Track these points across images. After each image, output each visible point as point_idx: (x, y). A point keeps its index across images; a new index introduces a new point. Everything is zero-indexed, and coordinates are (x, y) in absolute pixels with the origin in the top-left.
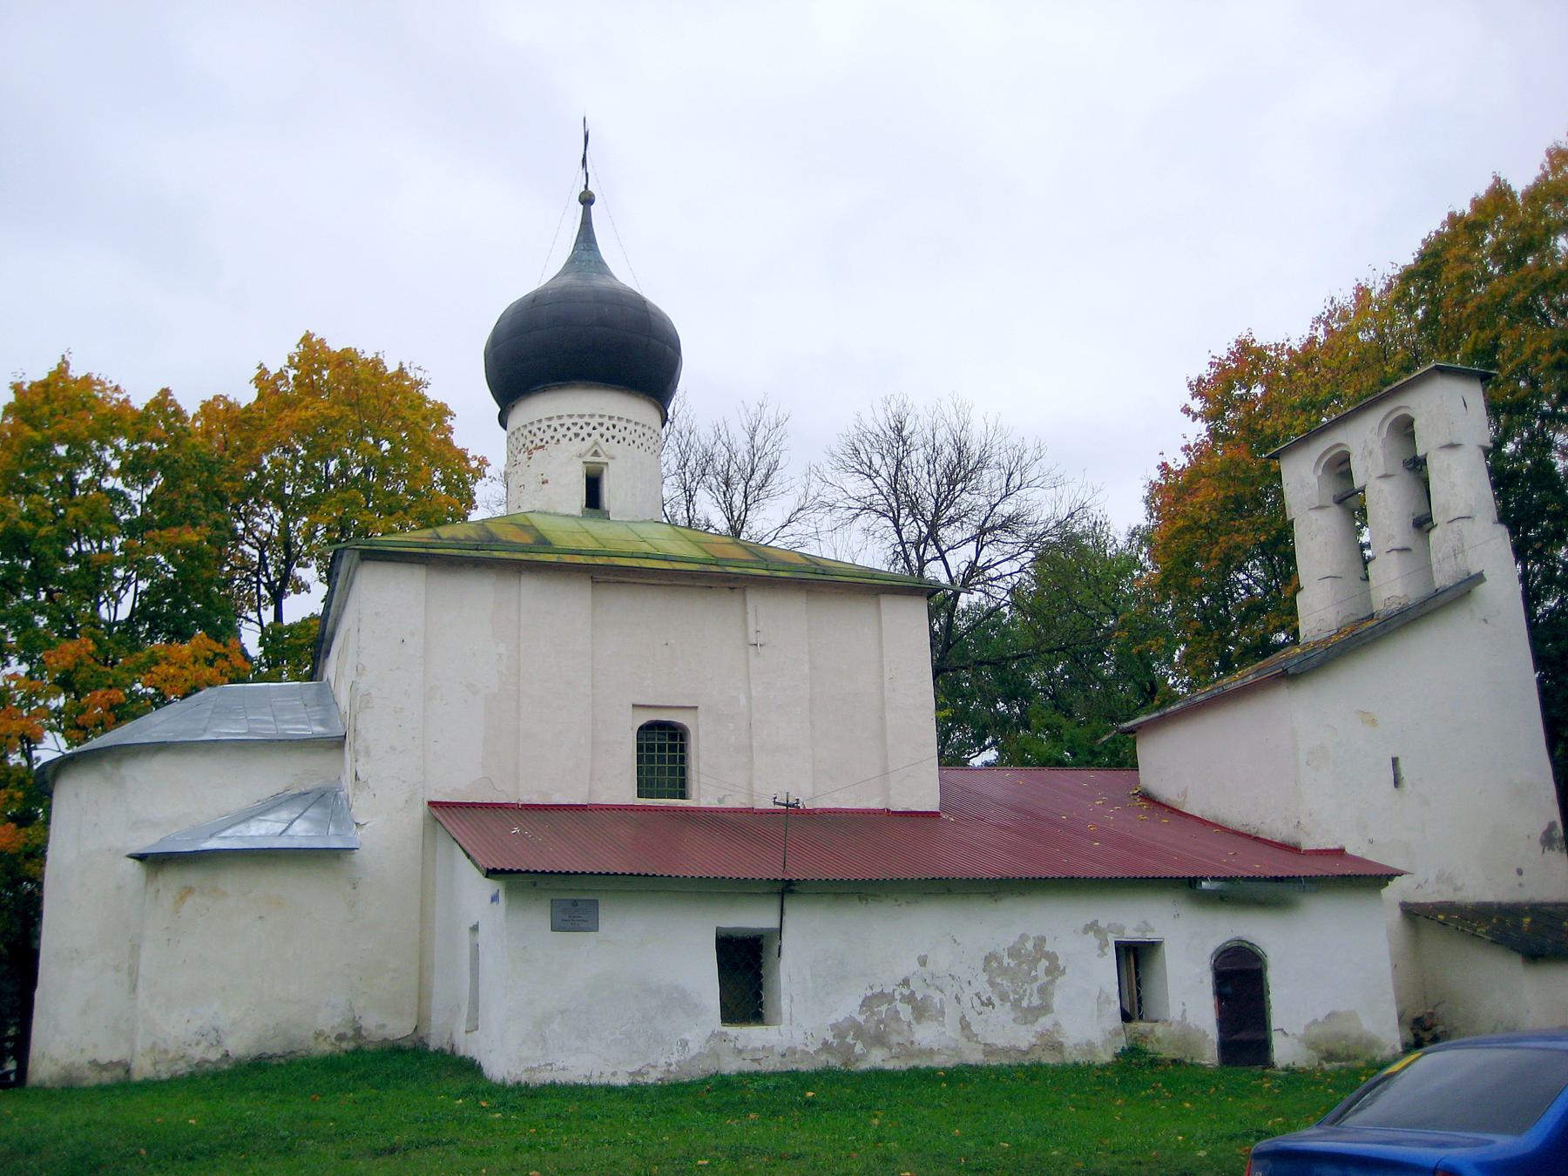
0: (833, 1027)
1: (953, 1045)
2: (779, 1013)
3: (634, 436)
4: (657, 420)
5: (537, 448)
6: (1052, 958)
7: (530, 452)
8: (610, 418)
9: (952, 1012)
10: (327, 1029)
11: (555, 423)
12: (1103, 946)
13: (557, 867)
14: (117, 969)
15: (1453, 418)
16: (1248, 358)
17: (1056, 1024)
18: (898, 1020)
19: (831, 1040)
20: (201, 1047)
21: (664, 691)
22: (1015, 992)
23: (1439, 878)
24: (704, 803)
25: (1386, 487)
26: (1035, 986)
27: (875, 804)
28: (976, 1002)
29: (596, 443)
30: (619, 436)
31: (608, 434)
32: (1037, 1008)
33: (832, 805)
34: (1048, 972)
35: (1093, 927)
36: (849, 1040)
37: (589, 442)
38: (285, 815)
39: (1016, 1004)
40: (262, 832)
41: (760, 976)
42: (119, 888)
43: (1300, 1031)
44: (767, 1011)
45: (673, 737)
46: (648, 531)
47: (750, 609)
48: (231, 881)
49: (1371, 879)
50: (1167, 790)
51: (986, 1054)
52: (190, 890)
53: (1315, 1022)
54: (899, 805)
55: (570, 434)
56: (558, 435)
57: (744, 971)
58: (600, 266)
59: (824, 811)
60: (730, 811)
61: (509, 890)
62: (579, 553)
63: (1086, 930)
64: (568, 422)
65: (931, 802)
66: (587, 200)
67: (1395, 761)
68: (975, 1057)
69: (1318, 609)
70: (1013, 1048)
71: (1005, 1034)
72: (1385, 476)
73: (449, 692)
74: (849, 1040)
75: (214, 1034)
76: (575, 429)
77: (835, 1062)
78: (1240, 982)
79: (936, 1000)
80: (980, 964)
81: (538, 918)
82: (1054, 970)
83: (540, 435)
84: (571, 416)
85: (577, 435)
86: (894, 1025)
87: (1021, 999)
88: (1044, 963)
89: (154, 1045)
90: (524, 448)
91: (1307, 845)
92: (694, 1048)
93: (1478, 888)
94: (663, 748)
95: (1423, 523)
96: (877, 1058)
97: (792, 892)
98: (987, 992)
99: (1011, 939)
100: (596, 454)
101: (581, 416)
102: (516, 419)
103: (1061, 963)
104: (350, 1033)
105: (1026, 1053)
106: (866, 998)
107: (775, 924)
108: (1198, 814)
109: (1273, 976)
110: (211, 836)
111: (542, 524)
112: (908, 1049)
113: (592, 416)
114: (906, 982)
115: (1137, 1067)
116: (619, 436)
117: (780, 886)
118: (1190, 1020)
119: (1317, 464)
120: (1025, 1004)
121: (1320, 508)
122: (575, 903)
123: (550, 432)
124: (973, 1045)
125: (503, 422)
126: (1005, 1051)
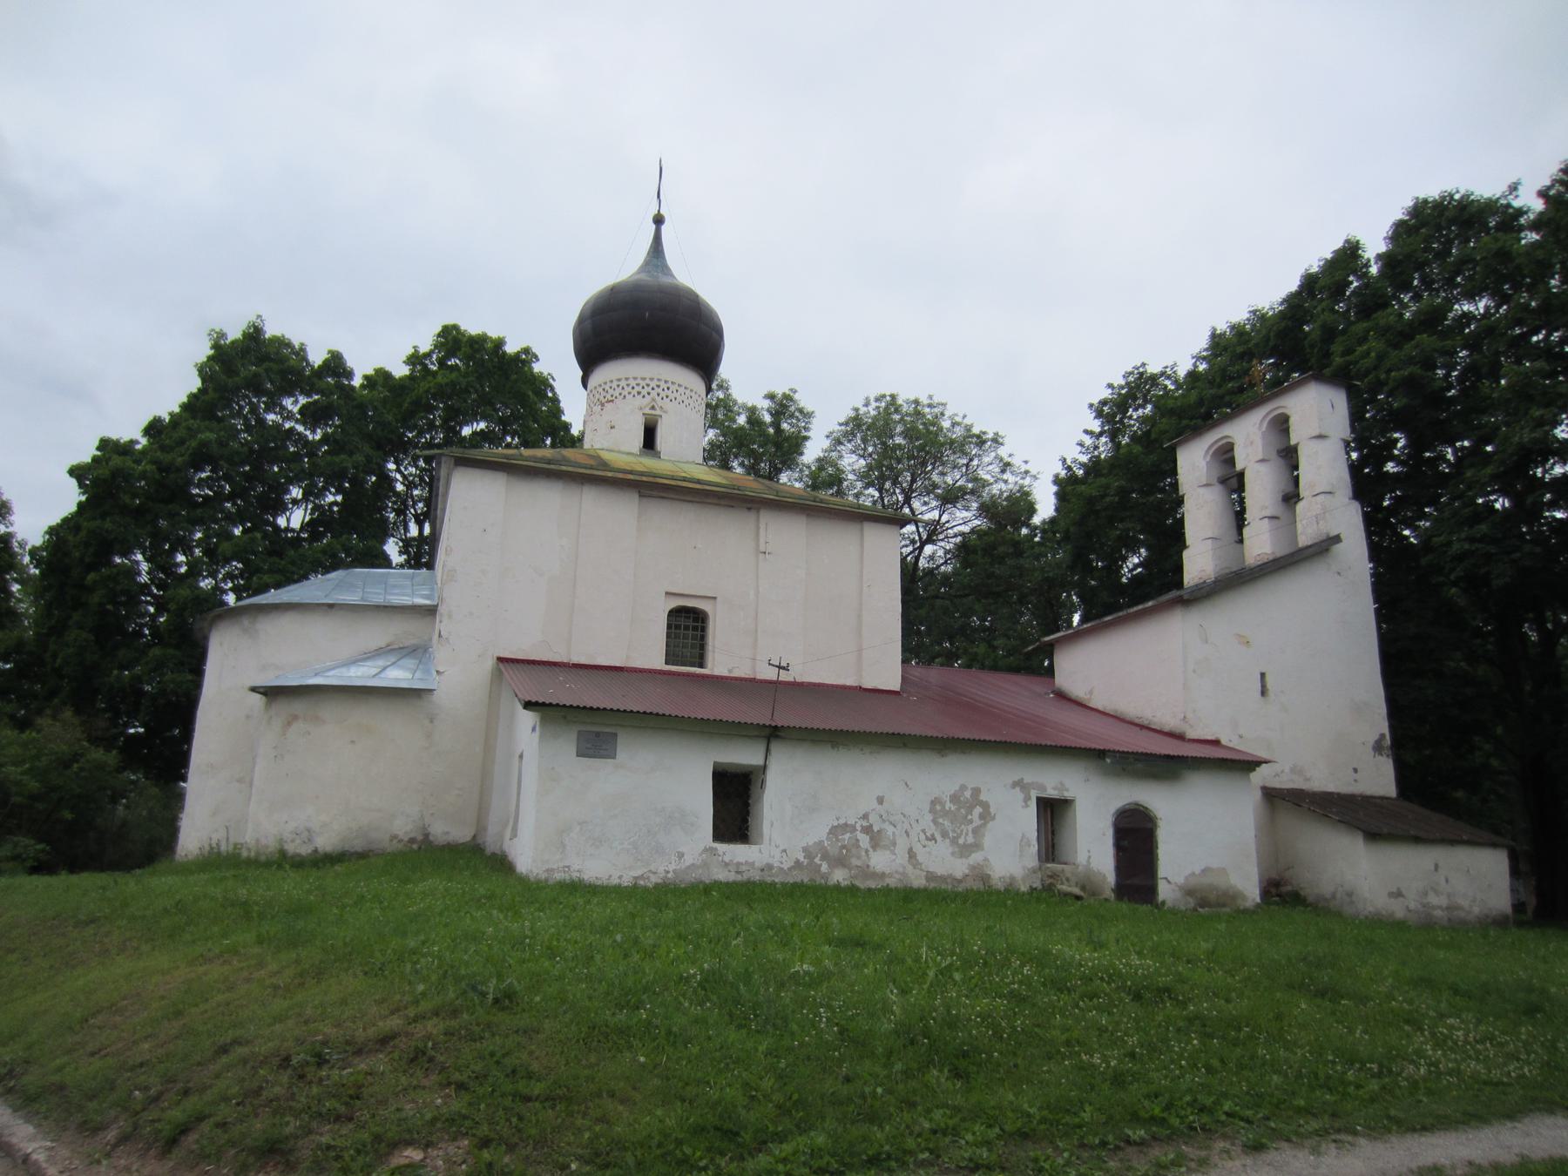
0: (805, 850)
2: (761, 835)
3: (684, 398)
6: (985, 806)
9: (902, 845)
11: (623, 383)
12: (1027, 799)
13: (588, 711)
15: (1318, 413)
17: (986, 860)
21: (692, 584)
23: (1293, 770)
24: (716, 673)
25: (1263, 468)
26: (970, 828)
27: (850, 681)
28: (922, 837)
30: (672, 396)
31: (663, 394)
32: (971, 845)
34: (982, 817)
36: (817, 860)
38: (381, 663)
39: (954, 841)
41: (747, 805)
43: (1181, 880)
44: (752, 833)
45: (696, 620)
46: (686, 467)
47: (762, 527)
48: (330, 711)
49: (1245, 765)
50: (1077, 690)
52: (295, 718)
54: (869, 683)
56: (625, 393)
57: (735, 804)
58: (665, 269)
60: (736, 679)
62: (631, 472)
63: (1015, 784)
64: (633, 383)
65: (895, 684)
66: (659, 220)
67: (1263, 675)
68: (918, 881)
69: (1198, 563)
70: (950, 876)
71: (944, 862)
72: (1262, 461)
73: (513, 567)
74: (817, 860)
76: (637, 389)
78: (1135, 837)
79: (890, 833)
81: (566, 745)
82: (986, 816)
87: (959, 837)
88: (978, 810)
90: (600, 403)
91: (1191, 734)
92: (689, 860)
93: (1322, 780)
94: (688, 627)
95: (1291, 498)
96: (839, 876)
97: (777, 737)
98: (931, 830)
99: (953, 788)
100: (653, 408)
102: (592, 382)
104: (420, 838)
105: (960, 881)
107: (761, 762)
111: (606, 456)
112: (866, 872)
114: (865, 817)
115: (1050, 897)
117: (767, 732)
120: (961, 841)
121: (1207, 485)
122: (598, 734)
123: (619, 390)
125: (585, 384)
126: (943, 879)
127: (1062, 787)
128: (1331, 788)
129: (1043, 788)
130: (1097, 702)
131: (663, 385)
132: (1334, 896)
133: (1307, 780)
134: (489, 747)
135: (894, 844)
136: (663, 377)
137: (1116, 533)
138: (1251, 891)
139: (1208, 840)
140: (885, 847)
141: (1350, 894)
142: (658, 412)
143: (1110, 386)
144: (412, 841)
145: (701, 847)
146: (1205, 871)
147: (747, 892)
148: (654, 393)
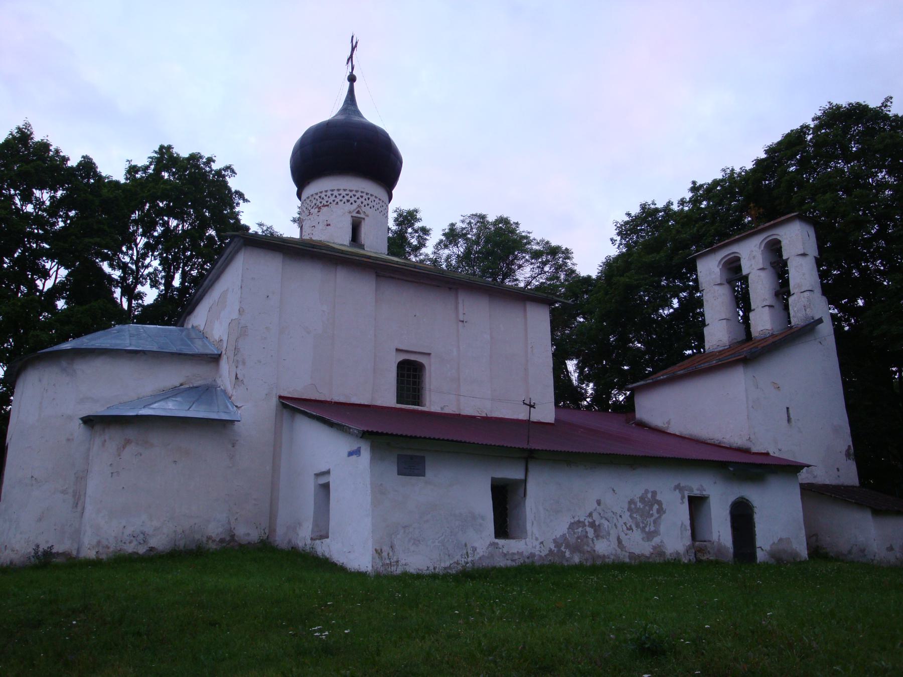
0: (555, 541)
1: (614, 552)
4: (386, 198)
5: (324, 206)
6: (659, 503)
7: (320, 208)
8: (367, 194)
10: (214, 535)
11: (336, 193)
12: (683, 498)
14: (64, 492)
16: (648, 214)
18: (587, 537)
19: (553, 548)
20: (133, 545)
22: (643, 523)
25: (763, 274)
26: (652, 519)
28: (625, 528)
29: (359, 206)
31: (365, 203)
33: (501, 416)
34: (659, 511)
35: (678, 487)
37: (355, 206)
40: (170, 408)
42: (68, 440)
47: (460, 301)
48: (157, 438)
49: (791, 469)
50: (657, 421)
51: (630, 558)
52: (128, 442)
53: (774, 543)
55: (345, 200)
56: (337, 200)
58: (358, 113)
59: (496, 418)
61: (374, 448)
64: (336, 193)
66: (352, 79)
67: (788, 408)
69: (718, 332)
71: (638, 545)
74: (563, 549)
75: (142, 536)
76: (347, 198)
77: (557, 560)
78: (742, 517)
79: (606, 526)
80: (626, 506)
82: (661, 511)
83: (326, 199)
84: (345, 190)
85: (348, 201)
86: (585, 540)
88: (656, 507)
89: (99, 543)
92: (481, 552)
94: (410, 375)
101: (351, 191)
103: (664, 506)
104: (228, 538)
106: (572, 524)
108: (678, 433)
109: (757, 518)
110: (144, 407)
112: (594, 555)
113: (357, 191)
114: (590, 515)
115: (700, 563)
116: (371, 204)
118: (722, 541)
119: (720, 262)
122: (412, 457)
123: (333, 198)
124: (624, 553)
127: (701, 489)
128: (827, 482)
129: (691, 490)
130: (674, 429)
131: (365, 196)
132: (850, 552)
133: (815, 477)
134: (275, 469)
135: (609, 534)
136: (366, 191)
137: (634, 313)
138: (803, 552)
139: (780, 519)
140: (603, 537)
141: (863, 551)
142: (362, 216)
143: (629, 214)
144: (222, 541)
145: (488, 543)
146: (781, 540)
147: (527, 572)
148: (359, 202)
